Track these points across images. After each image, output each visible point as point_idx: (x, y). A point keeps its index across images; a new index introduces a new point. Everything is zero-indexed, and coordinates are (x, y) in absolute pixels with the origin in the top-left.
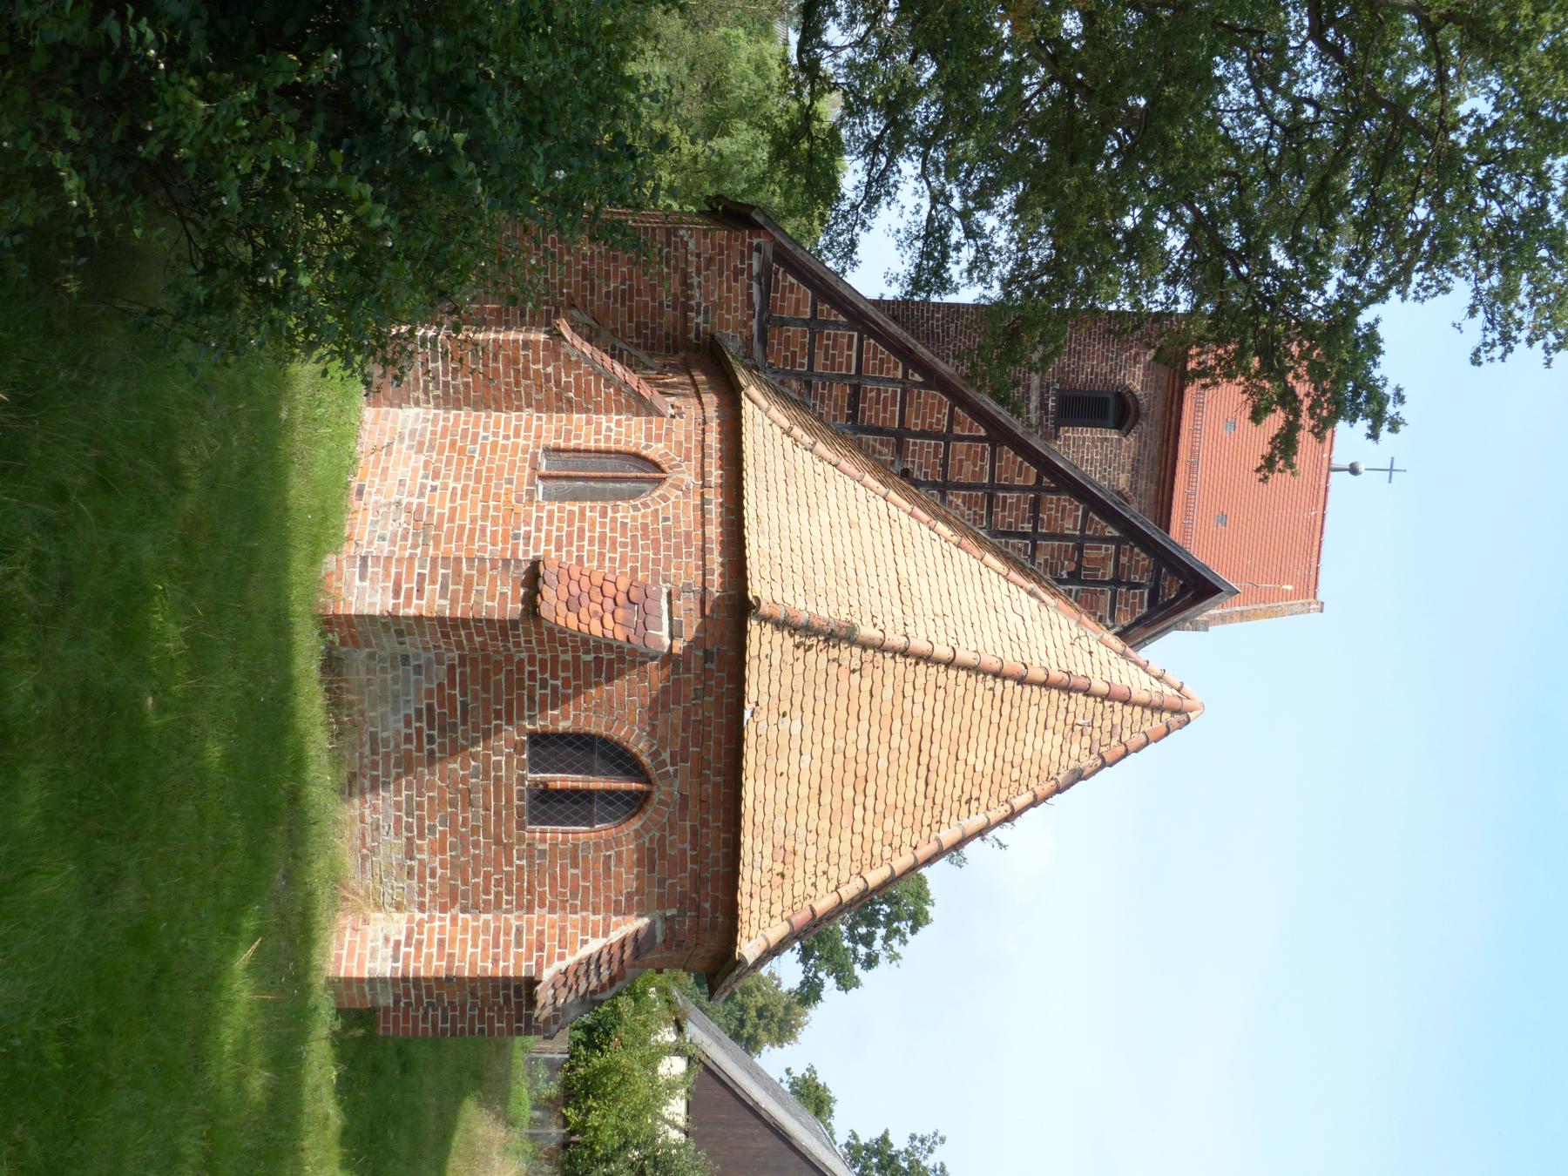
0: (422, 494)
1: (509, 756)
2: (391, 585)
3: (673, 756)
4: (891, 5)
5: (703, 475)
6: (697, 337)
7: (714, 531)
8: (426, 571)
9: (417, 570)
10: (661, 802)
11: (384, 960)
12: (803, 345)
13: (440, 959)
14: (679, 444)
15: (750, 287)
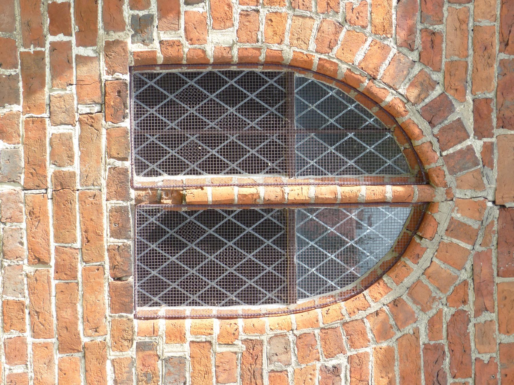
1: (88, 122)
3: (480, 111)
4: (31, 383)
10: (455, 228)
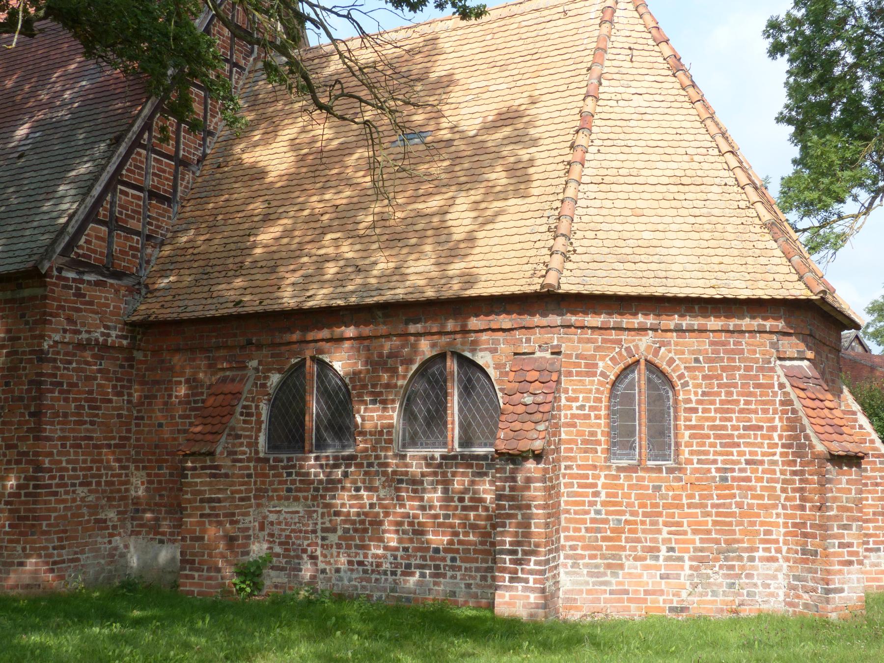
0: (681, 559)
2: (846, 568)
5: (642, 330)
6: (125, 337)
7: (714, 323)
8: (836, 542)
9: (837, 549)
11: (879, 557)
12: (126, 239)
13: (877, 521)
14: (597, 349)
15: (89, 282)
